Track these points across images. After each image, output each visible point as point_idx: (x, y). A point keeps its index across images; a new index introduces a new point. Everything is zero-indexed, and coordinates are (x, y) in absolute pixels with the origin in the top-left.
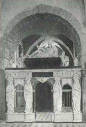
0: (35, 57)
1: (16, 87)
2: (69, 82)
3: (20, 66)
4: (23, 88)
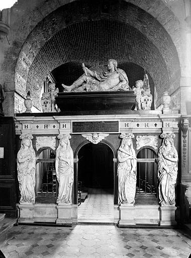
0: (81, 90)
1: (38, 153)
2: (50, 143)
3: (48, 110)
4: (53, 155)
